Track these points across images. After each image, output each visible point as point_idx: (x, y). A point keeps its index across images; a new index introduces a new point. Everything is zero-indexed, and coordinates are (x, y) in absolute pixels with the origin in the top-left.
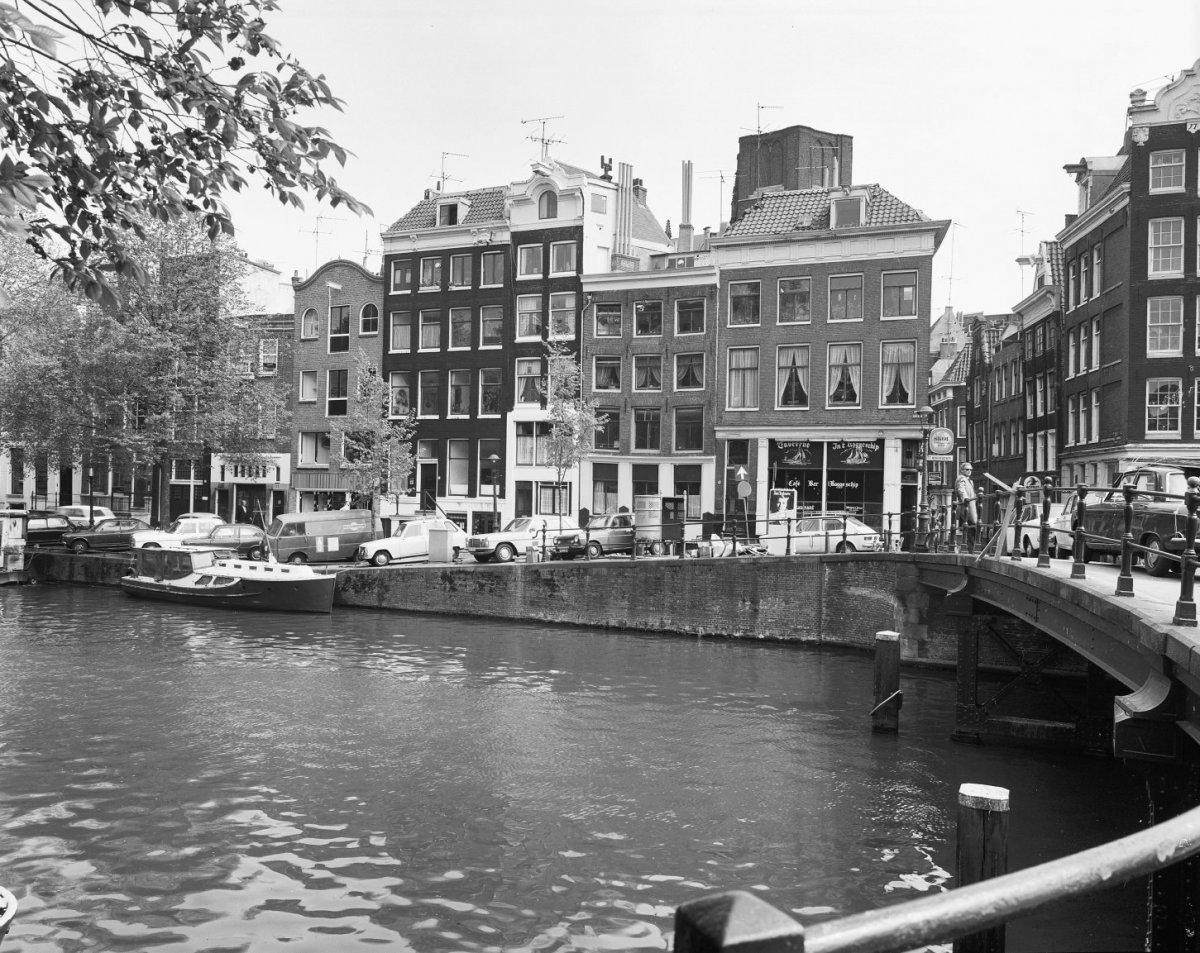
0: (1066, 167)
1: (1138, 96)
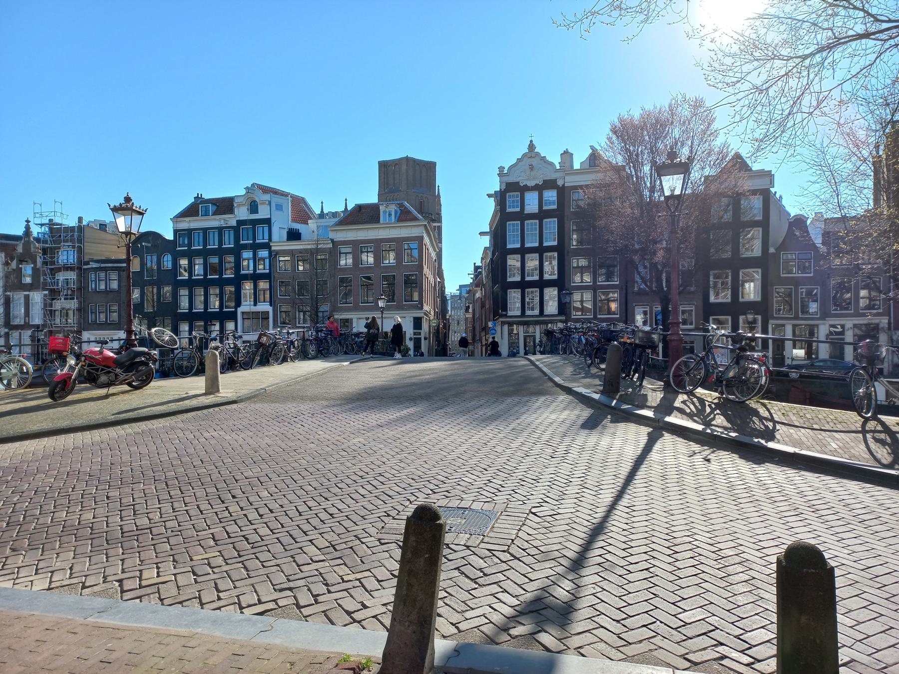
0: (487, 195)
1: (501, 169)
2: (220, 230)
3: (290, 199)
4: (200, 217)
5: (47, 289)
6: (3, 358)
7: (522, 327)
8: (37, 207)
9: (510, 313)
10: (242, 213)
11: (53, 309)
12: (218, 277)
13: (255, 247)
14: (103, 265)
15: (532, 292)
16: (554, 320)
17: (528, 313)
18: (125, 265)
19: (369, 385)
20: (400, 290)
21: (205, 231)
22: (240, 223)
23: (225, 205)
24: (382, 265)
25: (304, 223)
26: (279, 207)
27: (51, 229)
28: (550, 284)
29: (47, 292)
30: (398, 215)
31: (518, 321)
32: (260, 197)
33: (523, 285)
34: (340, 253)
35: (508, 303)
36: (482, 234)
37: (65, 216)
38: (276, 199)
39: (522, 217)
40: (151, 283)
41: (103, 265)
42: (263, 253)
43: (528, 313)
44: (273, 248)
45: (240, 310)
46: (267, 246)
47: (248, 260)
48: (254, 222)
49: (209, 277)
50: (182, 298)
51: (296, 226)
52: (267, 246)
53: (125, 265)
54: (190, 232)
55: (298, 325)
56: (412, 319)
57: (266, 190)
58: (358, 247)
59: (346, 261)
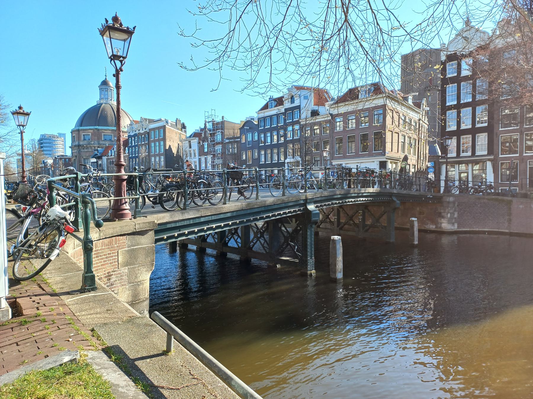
2: (277, 115)
4: (269, 110)
5: (212, 155)
7: (457, 166)
8: (206, 113)
9: (449, 156)
10: (287, 105)
11: (215, 164)
12: (518, 155)
13: (293, 124)
14: (231, 140)
15: (466, 138)
16: (484, 159)
18: (239, 140)
20: (371, 143)
21: (271, 117)
23: (279, 101)
24: (360, 127)
25: (322, 106)
27: (213, 124)
28: (482, 130)
29: (212, 156)
31: (453, 161)
32: (295, 92)
33: (459, 133)
34: (348, 120)
35: (476, 146)
36: (223, 117)
37: (217, 117)
38: (303, 93)
39: (458, 80)
40: (250, 148)
42: (297, 127)
43: (462, 155)
44: (302, 123)
45: (286, 161)
46: (298, 122)
47: (298, 131)
48: (292, 109)
51: (316, 108)
52: (298, 122)
53: (239, 140)
54: (264, 118)
56: (378, 163)
58: (345, 116)
59: (339, 125)
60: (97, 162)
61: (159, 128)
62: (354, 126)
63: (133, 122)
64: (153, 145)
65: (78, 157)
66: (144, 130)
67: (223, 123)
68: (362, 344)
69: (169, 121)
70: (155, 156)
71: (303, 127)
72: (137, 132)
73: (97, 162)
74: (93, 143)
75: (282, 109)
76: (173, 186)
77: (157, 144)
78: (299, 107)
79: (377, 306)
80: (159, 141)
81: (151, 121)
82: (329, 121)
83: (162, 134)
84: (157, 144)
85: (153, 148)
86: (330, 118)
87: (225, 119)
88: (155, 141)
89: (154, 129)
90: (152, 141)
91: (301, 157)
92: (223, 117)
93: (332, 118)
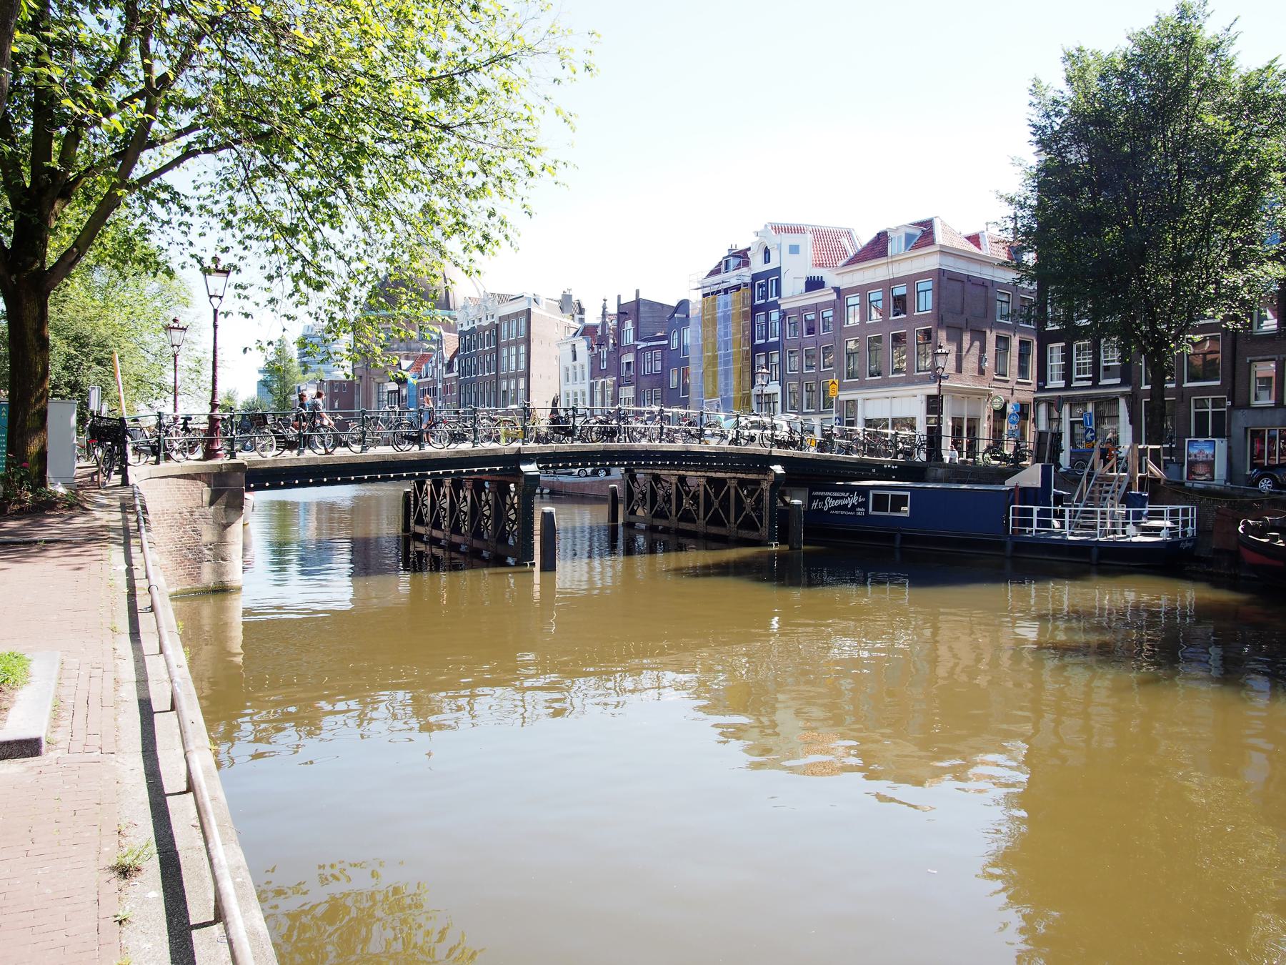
3: (810, 236)
6: (166, 5)
10: (758, 265)
12: (1218, 383)
14: (649, 344)
17: (1051, 385)
18: (666, 342)
19: (1086, 583)
22: (755, 277)
23: (742, 257)
24: (868, 322)
26: (794, 249)
30: (732, 278)
36: (637, 292)
41: (649, 344)
44: (782, 308)
49: (1186, 385)
50: (986, 436)
51: (817, 272)
53: (666, 342)
55: (805, 410)
56: (924, 398)
57: (780, 229)
60: (399, 391)
61: (517, 315)
62: (857, 319)
63: (244, 399)
64: (505, 353)
65: (364, 378)
66: (490, 320)
67: (638, 302)
68: (303, 583)
69: (542, 299)
70: (508, 377)
71: (785, 316)
72: (477, 323)
73: (399, 391)
74: (395, 346)
75: (746, 275)
76: (1158, 379)
77: (514, 351)
78: (777, 271)
79: (322, 561)
80: (517, 343)
81: (503, 299)
82: (833, 305)
83: (523, 330)
84: (514, 351)
85: (506, 359)
86: (834, 297)
87: (641, 296)
88: (508, 345)
89: (508, 317)
90: (508, 345)
91: (782, 382)
92: (637, 292)
93: (839, 296)
